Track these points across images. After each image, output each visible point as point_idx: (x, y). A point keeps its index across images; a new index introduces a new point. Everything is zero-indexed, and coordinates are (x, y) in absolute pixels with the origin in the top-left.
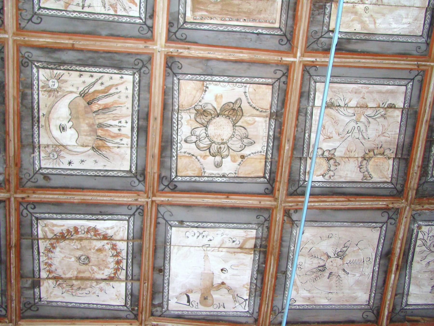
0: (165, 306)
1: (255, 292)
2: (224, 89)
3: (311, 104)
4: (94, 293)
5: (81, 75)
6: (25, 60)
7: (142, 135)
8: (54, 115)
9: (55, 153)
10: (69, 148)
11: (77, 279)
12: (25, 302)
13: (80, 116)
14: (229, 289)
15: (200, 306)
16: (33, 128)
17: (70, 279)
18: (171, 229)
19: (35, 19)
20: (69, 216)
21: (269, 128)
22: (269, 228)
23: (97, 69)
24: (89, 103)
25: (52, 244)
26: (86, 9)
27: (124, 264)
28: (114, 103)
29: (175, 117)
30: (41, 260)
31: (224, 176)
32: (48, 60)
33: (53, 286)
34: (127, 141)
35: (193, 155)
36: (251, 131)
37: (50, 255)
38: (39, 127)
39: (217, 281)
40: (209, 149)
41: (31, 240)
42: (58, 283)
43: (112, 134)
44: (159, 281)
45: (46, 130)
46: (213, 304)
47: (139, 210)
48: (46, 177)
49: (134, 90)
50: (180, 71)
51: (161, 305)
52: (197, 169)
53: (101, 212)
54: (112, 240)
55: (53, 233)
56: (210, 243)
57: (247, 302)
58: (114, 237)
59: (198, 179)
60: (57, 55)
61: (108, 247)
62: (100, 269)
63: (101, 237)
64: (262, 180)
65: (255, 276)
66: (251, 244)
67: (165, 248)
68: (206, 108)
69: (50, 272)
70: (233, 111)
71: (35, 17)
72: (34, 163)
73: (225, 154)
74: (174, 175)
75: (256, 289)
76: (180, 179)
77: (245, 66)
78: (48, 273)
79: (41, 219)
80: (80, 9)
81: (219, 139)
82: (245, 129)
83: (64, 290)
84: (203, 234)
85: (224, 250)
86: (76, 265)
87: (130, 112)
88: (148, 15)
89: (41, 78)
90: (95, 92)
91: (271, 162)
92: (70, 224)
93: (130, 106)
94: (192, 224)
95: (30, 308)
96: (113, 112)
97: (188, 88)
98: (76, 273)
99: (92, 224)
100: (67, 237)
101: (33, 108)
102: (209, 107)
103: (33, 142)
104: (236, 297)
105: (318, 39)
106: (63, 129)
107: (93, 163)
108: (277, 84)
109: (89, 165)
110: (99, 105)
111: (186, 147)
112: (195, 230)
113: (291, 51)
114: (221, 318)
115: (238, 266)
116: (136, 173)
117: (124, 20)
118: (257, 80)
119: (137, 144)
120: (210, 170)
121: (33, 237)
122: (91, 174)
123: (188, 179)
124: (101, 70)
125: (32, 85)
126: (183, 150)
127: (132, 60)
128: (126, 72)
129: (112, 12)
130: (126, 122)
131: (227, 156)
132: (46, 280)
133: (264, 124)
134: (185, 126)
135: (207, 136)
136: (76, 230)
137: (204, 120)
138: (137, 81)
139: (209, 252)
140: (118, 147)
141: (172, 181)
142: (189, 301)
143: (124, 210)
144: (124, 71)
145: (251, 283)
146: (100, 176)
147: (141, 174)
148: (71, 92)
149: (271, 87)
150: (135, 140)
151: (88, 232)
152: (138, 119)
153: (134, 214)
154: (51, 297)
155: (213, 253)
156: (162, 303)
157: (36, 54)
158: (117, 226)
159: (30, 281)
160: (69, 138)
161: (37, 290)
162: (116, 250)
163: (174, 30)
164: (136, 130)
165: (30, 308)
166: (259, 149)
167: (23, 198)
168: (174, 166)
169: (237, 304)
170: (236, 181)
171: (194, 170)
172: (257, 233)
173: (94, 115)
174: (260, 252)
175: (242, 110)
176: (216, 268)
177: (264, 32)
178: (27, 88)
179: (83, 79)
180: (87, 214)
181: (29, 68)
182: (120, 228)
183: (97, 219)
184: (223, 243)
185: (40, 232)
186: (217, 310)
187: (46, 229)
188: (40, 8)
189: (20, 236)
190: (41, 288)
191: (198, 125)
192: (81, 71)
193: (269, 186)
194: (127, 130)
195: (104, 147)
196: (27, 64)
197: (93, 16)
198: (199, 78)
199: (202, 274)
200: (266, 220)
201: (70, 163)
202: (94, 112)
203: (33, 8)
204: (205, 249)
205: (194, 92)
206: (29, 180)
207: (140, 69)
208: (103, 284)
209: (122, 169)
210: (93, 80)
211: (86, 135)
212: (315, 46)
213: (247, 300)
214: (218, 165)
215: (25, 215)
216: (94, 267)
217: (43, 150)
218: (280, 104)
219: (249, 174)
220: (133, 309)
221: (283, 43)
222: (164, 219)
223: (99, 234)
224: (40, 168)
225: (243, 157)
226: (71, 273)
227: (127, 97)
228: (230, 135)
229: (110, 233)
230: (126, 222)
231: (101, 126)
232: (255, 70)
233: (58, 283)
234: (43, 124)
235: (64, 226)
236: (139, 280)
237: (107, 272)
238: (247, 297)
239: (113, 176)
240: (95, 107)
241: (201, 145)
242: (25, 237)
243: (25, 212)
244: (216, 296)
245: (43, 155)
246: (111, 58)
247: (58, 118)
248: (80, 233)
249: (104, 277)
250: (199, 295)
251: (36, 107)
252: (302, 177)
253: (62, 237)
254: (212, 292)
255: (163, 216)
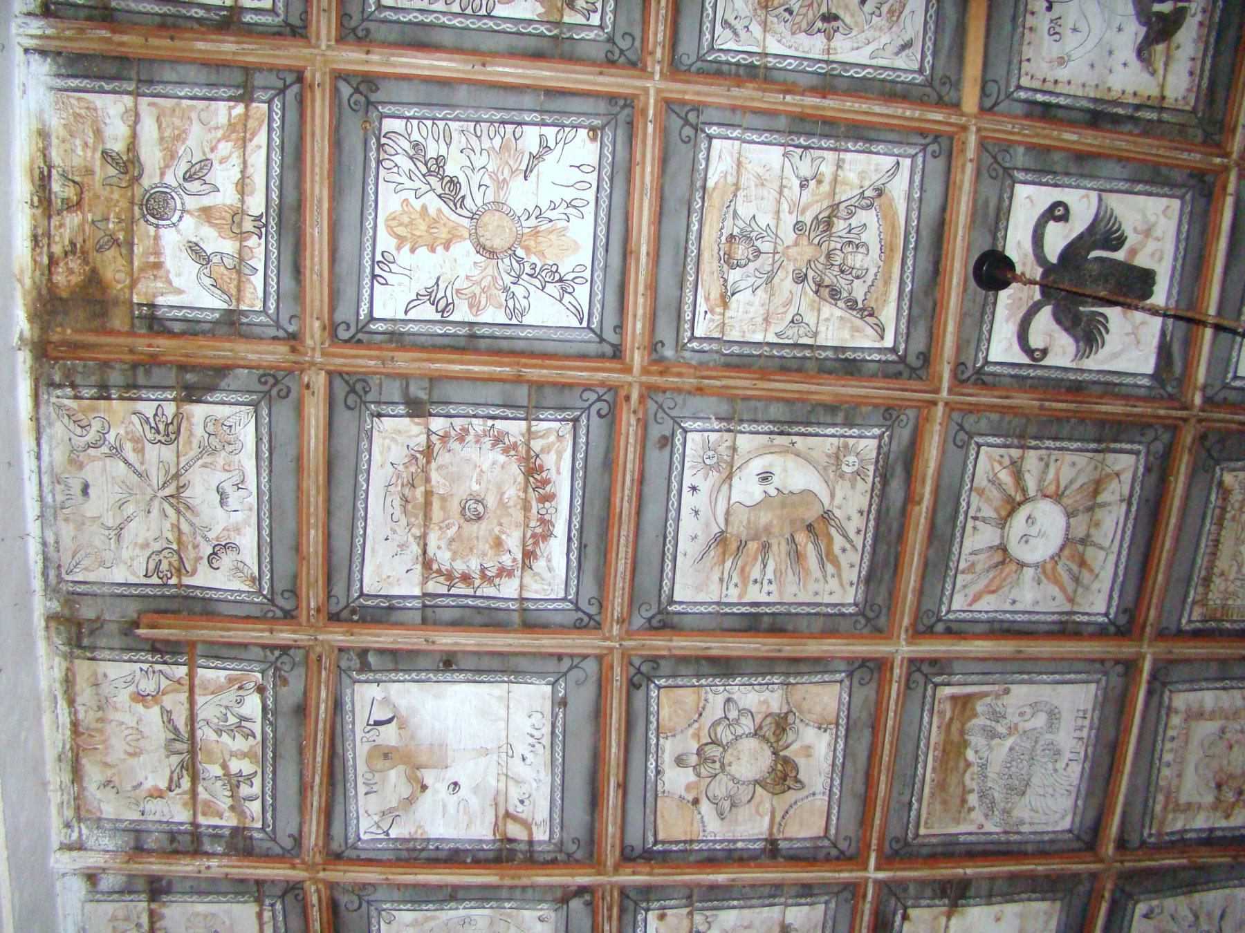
0: (363, 677)
1: (407, 850)
2: (822, 759)
3: (790, 901)
4: (394, 532)
5: (861, 512)
6: (895, 414)
7: (744, 623)
8: (791, 462)
9: (715, 460)
10: (725, 487)
11: (428, 494)
12: (370, 382)
13: (785, 511)
14: (410, 801)
15: (367, 746)
16: (770, 422)
17: (428, 480)
18: (548, 684)
19: (962, 435)
20: (579, 484)
21: (750, 841)
22: (554, 862)
23: (869, 541)
24: (810, 528)
25: (515, 446)
26: (970, 523)
27: (461, 589)
28: (808, 572)
29: (776, 679)
30: (475, 421)
31: (658, 772)
32: (892, 456)
33: (412, 445)
34: (733, 595)
35: (700, 715)
36: (744, 812)
37: (487, 442)
38: (771, 433)
39: (429, 777)
40: (713, 743)
41: (525, 404)
42: (418, 455)
43: (748, 569)
44: (422, 662)
45: (765, 447)
46: (372, 771)
47: (586, 619)
48: (666, 441)
49: (827, 605)
50: (856, 684)
51: (365, 667)
52: (672, 724)
53: (586, 546)
54: (523, 568)
55: (542, 450)
56: (517, 759)
57: (382, 836)
58: (528, 572)
59: (653, 726)
60: (899, 470)
61: (507, 560)
62: (452, 540)
63: (530, 548)
64: (651, 839)
65: (444, 846)
66: (514, 830)
67: (503, 672)
68: (790, 732)
69: (445, 438)
70: (784, 775)
71: (966, 438)
72: (696, 418)
73: (703, 770)
74: (662, 682)
75: (414, 849)
76: (654, 694)
77: (860, 788)
78: (441, 433)
79: (574, 427)
80: (972, 513)
81: (732, 759)
82: (749, 801)
83: (401, 468)
84: (537, 746)
85: (502, 785)
86: (461, 492)
87: (788, 599)
88: (953, 625)
89: (863, 443)
90: (830, 539)
91: (686, 851)
92: (562, 486)
93: (800, 599)
94: (559, 724)
95: (353, 390)
96: (790, 570)
97: (826, 699)
98: (442, 492)
99: (560, 529)
100: (531, 479)
101: (808, 424)
102: (791, 736)
103: (742, 421)
104: (392, 814)
105: (895, 895)
106: (765, 477)
107: (692, 532)
108: (826, 843)
109: (688, 524)
110: (806, 545)
111: (716, 701)
112: (547, 730)
113: (886, 861)
114: (339, 786)
115: (465, 812)
116: (668, 613)
117: (948, 586)
118: (835, 811)
119: (726, 614)
120: (670, 748)
121: (534, 411)
122: (669, 529)
123: (653, 708)
124: (868, 548)
125: (851, 426)
126: (710, 696)
127: (879, 600)
128: (860, 591)
129: (962, 566)
130: (769, 593)
131: (698, 775)
132: (424, 431)
133: (756, 831)
134: (757, 698)
135: (737, 738)
136: (549, 498)
137: (768, 731)
138: (844, 610)
139: (495, 757)
140: (721, 580)
141: (649, 679)
142: (377, 723)
143: (589, 590)
144: (862, 587)
145: (429, 840)
146: (664, 544)
147: (665, 623)
148: (832, 496)
149: (822, 834)
150: (735, 610)
151: (543, 521)
152: (773, 614)
153: (578, 609)
154: (384, 438)
155: (494, 764)
156: (371, 671)
157: (905, 434)
158: (554, 578)
159: (423, 395)
160: (747, 489)
161: (401, 409)
162: (499, 575)
163: (925, 668)
164: (753, 610)
165: (353, 390)
166: (710, 828)
167: (628, 398)
168: (679, 681)
169: (376, 818)
170: (648, 795)
171: (670, 719)
172: (541, 843)
173: (787, 536)
174: (500, 850)
175: (784, 792)
176: (463, 771)
177: (913, 813)
178: (846, 418)
179: (855, 516)
180: (582, 519)
181: (881, 421)
182: (550, 584)
183: (569, 539)
184: (517, 782)
185: (545, 425)
186: (360, 781)
187: (552, 438)
188: (979, 446)
189: (539, 386)
190: (408, 419)
191: (758, 720)
192: (869, 512)
193: (638, 851)
194: (754, 594)
195: (724, 553)
196: (888, 416)
197: (958, 535)
198: (843, 715)
199: (443, 746)
200: (569, 855)
201: (694, 489)
202: (792, 536)
203: (982, 435)
204: (504, 749)
205: (818, 709)
206: (661, 406)
207: (864, 615)
208: (416, 549)
209: (676, 586)
210: (852, 534)
211: (749, 522)
212: (885, 891)
213: (388, 835)
214: (680, 761)
215: (585, 396)
216: (455, 529)
217: (722, 437)
218: (792, 852)
219: (663, 816)
220: (353, 612)
221: (894, 844)
222: (570, 669)
223: (536, 543)
224: (685, 431)
225: (696, 802)
226: (442, 481)
227: (816, 594)
228: (738, 776)
229: (540, 565)
230: (562, 595)
231: (766, 547)
232: (852, 809)
233: (418, 455)
234: (776, 442)
235: (559, 473)
236: (424, 621)
237: (443, 557)
238: (393, 833)
239: (662, 571)
240: (801, 538)
241: (720, 729)
242: (534, 396)
243: (593, 397)
244: (395, 777)
245: (713, 436)
246: (886, 565)
247: (785, 470)
248: (541, 506)
249: (430, 552)
250: (393, 743)
251: (810, 430)
252: (656, 905)
253: (533, 470)
254: (401, 768)
255: (576, 666)
